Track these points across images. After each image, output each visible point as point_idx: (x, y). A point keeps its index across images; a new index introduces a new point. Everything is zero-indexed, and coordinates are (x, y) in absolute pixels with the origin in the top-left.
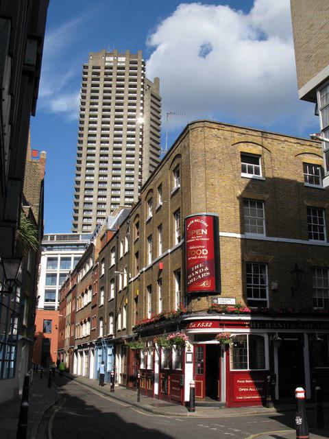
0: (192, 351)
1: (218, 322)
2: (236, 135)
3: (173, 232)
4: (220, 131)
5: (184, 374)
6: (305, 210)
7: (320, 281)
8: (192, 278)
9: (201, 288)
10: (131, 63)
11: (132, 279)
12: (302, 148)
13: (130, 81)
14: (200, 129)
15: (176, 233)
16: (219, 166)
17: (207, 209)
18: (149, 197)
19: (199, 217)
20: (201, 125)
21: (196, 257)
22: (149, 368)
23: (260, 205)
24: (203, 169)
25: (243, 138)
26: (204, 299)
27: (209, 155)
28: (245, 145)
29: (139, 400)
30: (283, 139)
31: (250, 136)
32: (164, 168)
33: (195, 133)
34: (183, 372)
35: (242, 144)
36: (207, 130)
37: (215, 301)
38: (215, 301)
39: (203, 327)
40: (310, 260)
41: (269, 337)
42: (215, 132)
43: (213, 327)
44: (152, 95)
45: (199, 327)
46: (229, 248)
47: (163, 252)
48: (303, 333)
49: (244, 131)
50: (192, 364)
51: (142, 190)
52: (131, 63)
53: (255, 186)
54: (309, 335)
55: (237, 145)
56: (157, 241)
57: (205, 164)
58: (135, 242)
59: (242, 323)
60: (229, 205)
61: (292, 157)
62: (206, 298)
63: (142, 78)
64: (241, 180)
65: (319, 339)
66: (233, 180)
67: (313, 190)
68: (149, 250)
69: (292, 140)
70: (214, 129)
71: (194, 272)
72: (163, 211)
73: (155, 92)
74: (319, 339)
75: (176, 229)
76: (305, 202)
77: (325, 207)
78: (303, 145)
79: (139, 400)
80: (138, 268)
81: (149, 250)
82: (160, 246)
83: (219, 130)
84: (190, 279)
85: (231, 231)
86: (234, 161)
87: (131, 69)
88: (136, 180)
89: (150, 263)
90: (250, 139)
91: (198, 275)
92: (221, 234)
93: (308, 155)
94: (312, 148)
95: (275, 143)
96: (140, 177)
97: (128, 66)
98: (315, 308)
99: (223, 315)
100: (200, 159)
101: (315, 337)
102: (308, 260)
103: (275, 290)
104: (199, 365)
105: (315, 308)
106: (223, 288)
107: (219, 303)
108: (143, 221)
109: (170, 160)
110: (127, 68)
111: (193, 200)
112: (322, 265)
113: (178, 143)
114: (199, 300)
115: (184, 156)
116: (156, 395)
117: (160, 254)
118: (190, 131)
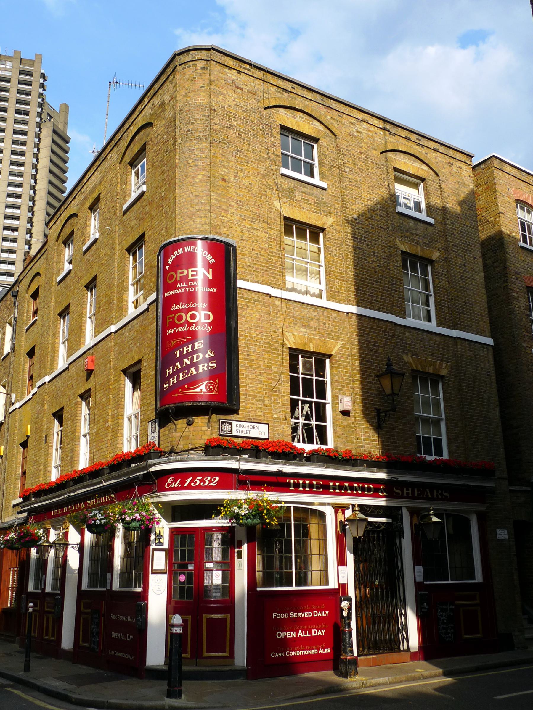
0: (166, 546)
1: (235, 476)
2: (273, 89)
3: (123, 289)
4: (243, 77)
5: (147, 599)
6: (399, 258)
7: (426, 403)
8: (176, 373)
9: (194, 397)
10: (21, 72)
11: (17, 405)
12: (391, 139)
13: (19, 83)
14: (200, 64)
15: (132, 289)
16: (238, 141)
17: (212, 227)
18: (67, 231)
19: (191, 241)
20: (204, 55)
21: (185, 329)
22: (48, 589)
23: (315, 239)
24: (204, 145)
25: (285, 99)
26: (200, 421)
27: (217, 118)
28: (289, 113)
29: (27, 668)
30: (360, 116)
31: (299, 99)
32: (106, 164)
33: (189, 72)
34: (144, 596)
35: (282, 110)
36: (216, 69)
37: (226, 428)
38: (226, 428)
39: (199, 487)
40: (408, 358)
41: (336, 512)
42: (231, 75)
43: (220, 486)
44: (54, 131)
45: (189, 487)
46: (256, 316)
47: (97, 332)
48: (400, 508)
49: (288, 86)
50: (166, 576)
51: (50, 221)
52: (21, 72)
53: (308, 197)
54: (413, 512)
55: (272, 110)
56: (82, 315)
57: (210, 136)
58: (27, 330)
59: (281, 479)
60: (256, 225)
61: (375, 154)
62: (205, 419)
63: (40, 100)
64: (280, 180)
65: (435, 519)
66: (264, 177)
67: (412, 223)
68: (61, 337)
69: (376, 122)
70: (230, 68)
71: (181, 361)
72: (102, 250)
73: (61, 126)
74: (435, 519)
75: (131, 281)
76: (399, 243)
77: (434, 258)
78: (395, 134)
79: (27, 668)
80: (31, 377)
81: (61, 337)
82: (89, 326)
83: (239, 72)
84: (172, 376)
85: (260, 280)
86: (270, 141)
87: (20, 82)
88: (20, 246)
89: (62, 363)
90: (299, 103)
91: (188, 367)
92: (240, 284)
93: (402, 155)
94: (410, 144)
95: (346, 120)
96: (29, 243)
97: (15, 77)
98: (419, 455)
99: (245, 460)
100: (200, 124)
101: (428, 516)
102: (405, 357)
103: (345, 413)
104: (182, 578)
105: (419, 455)
106: (244, 401)
107: (234, 433)
108: (49, 282)
109: (123, 144)
110: (14, 81)
111: (180, 208)
112: (431, 370)
113: (146, 100)
114: (189, 424)
115: (159, 127)
116: (66, 652)
117: (89, 340)
118: (179, 69)
